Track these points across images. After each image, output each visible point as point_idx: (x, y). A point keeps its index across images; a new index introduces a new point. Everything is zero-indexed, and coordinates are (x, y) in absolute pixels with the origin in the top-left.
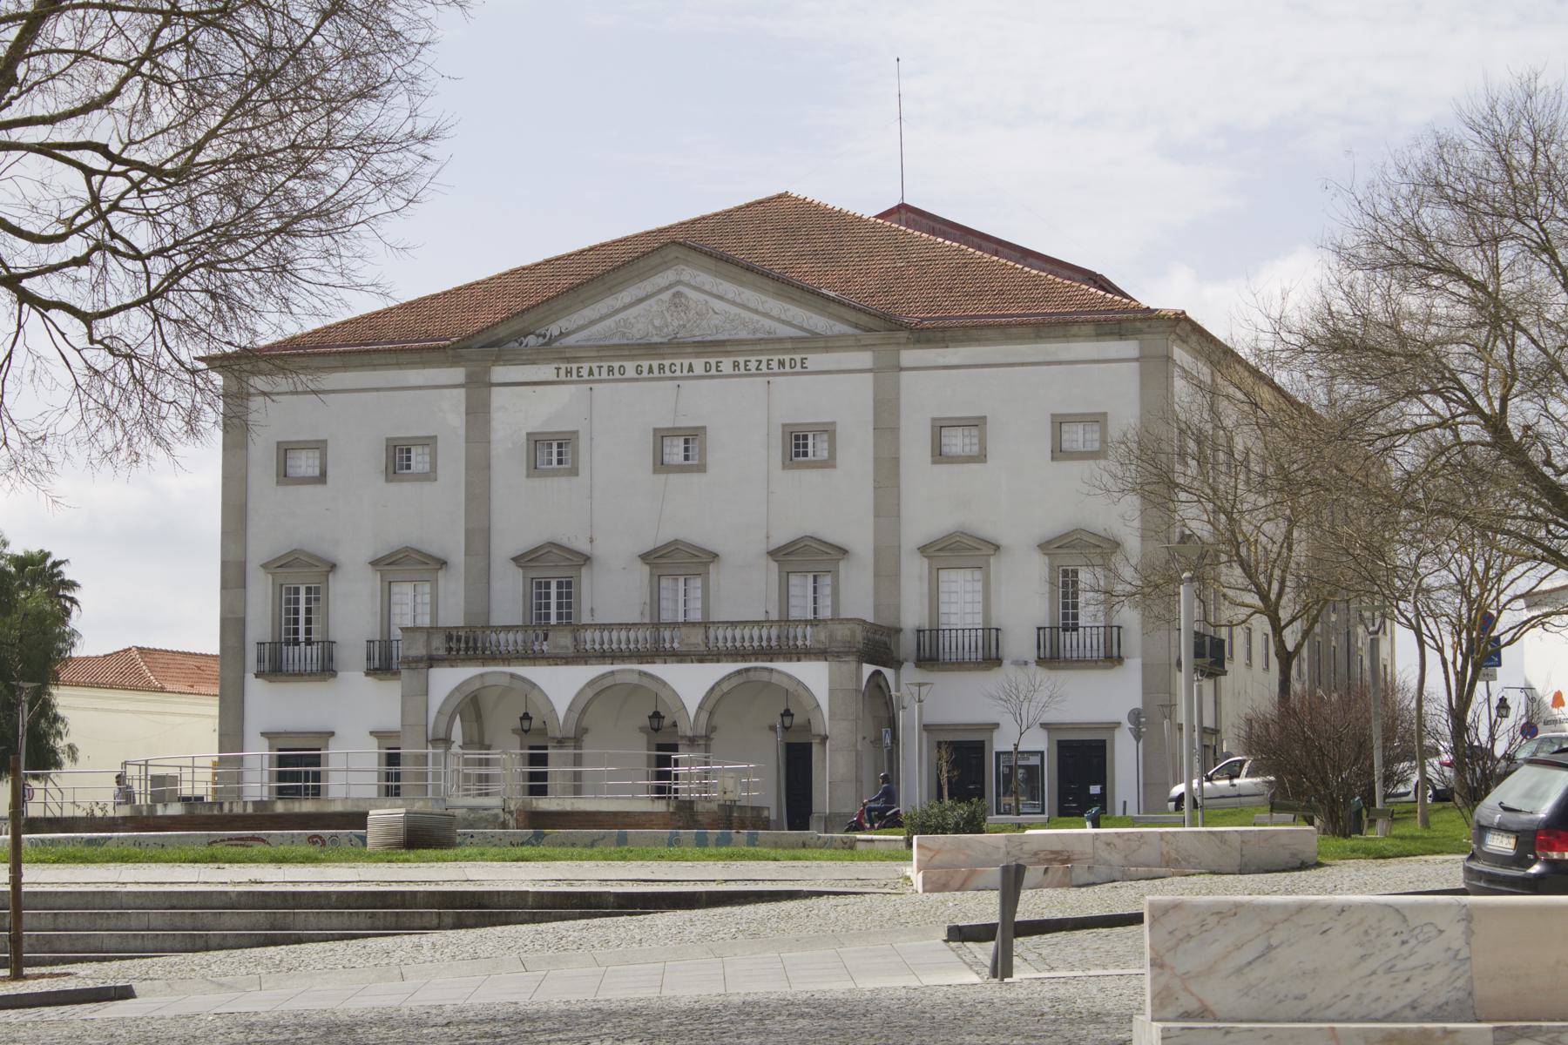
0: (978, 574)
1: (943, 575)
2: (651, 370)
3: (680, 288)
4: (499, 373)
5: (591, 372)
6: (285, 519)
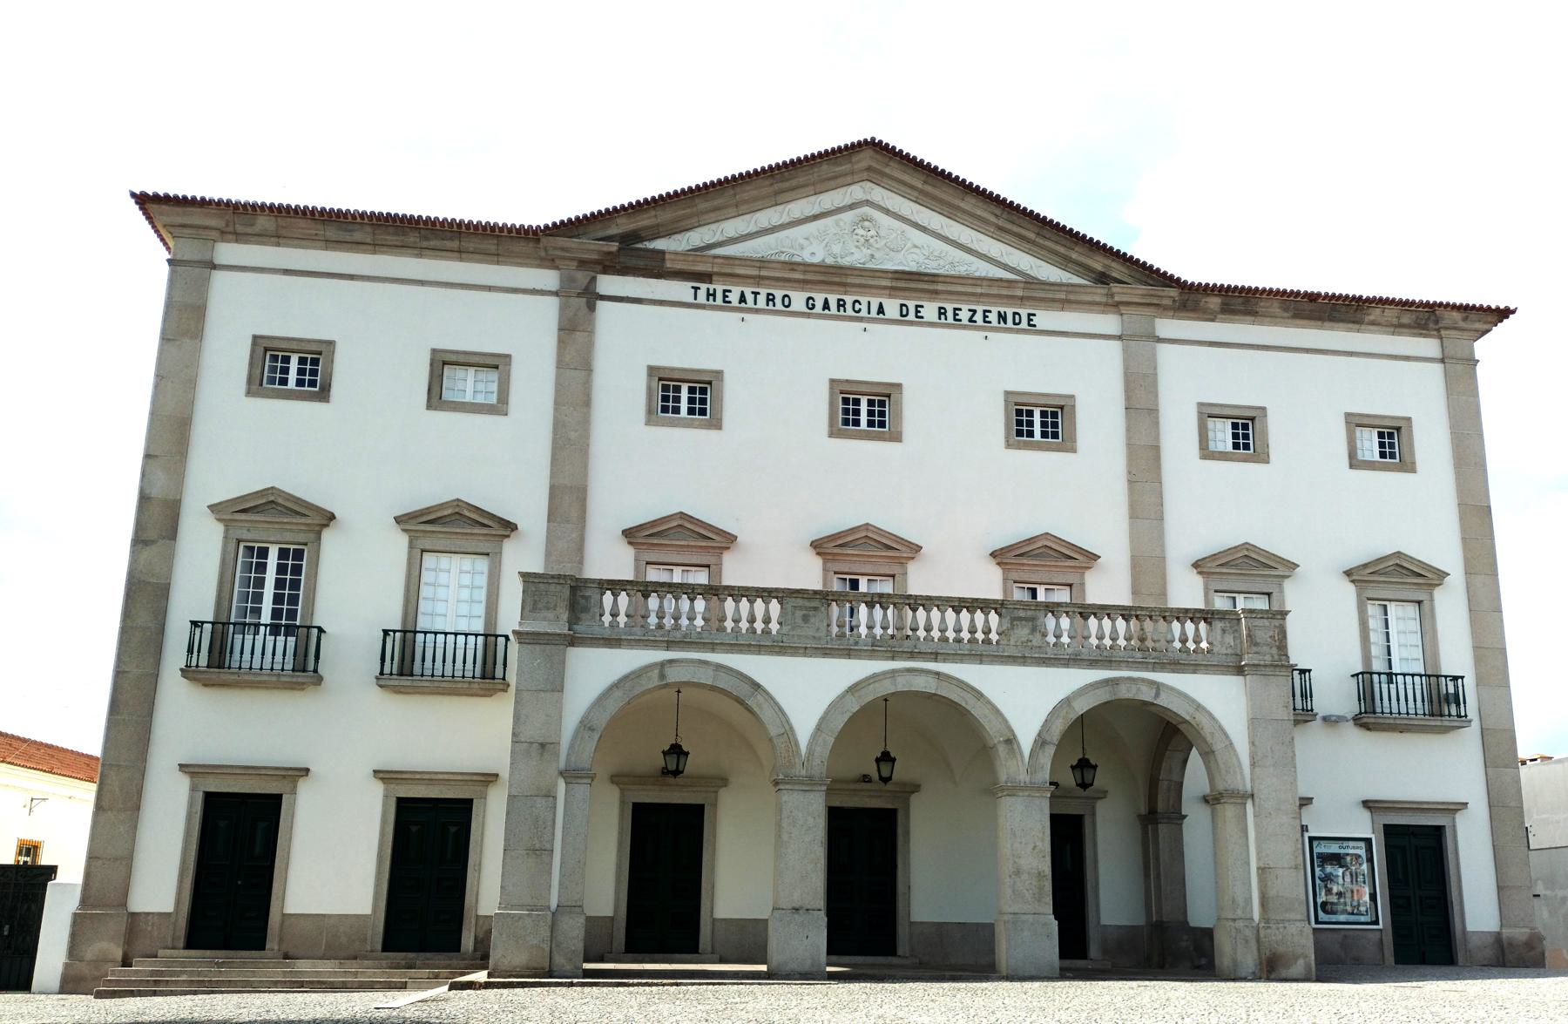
0: (482, 564)
1: (429, 560)
2: (826, 306)
3: (866, 210)
5: (743, 299)
6: (249, 441)
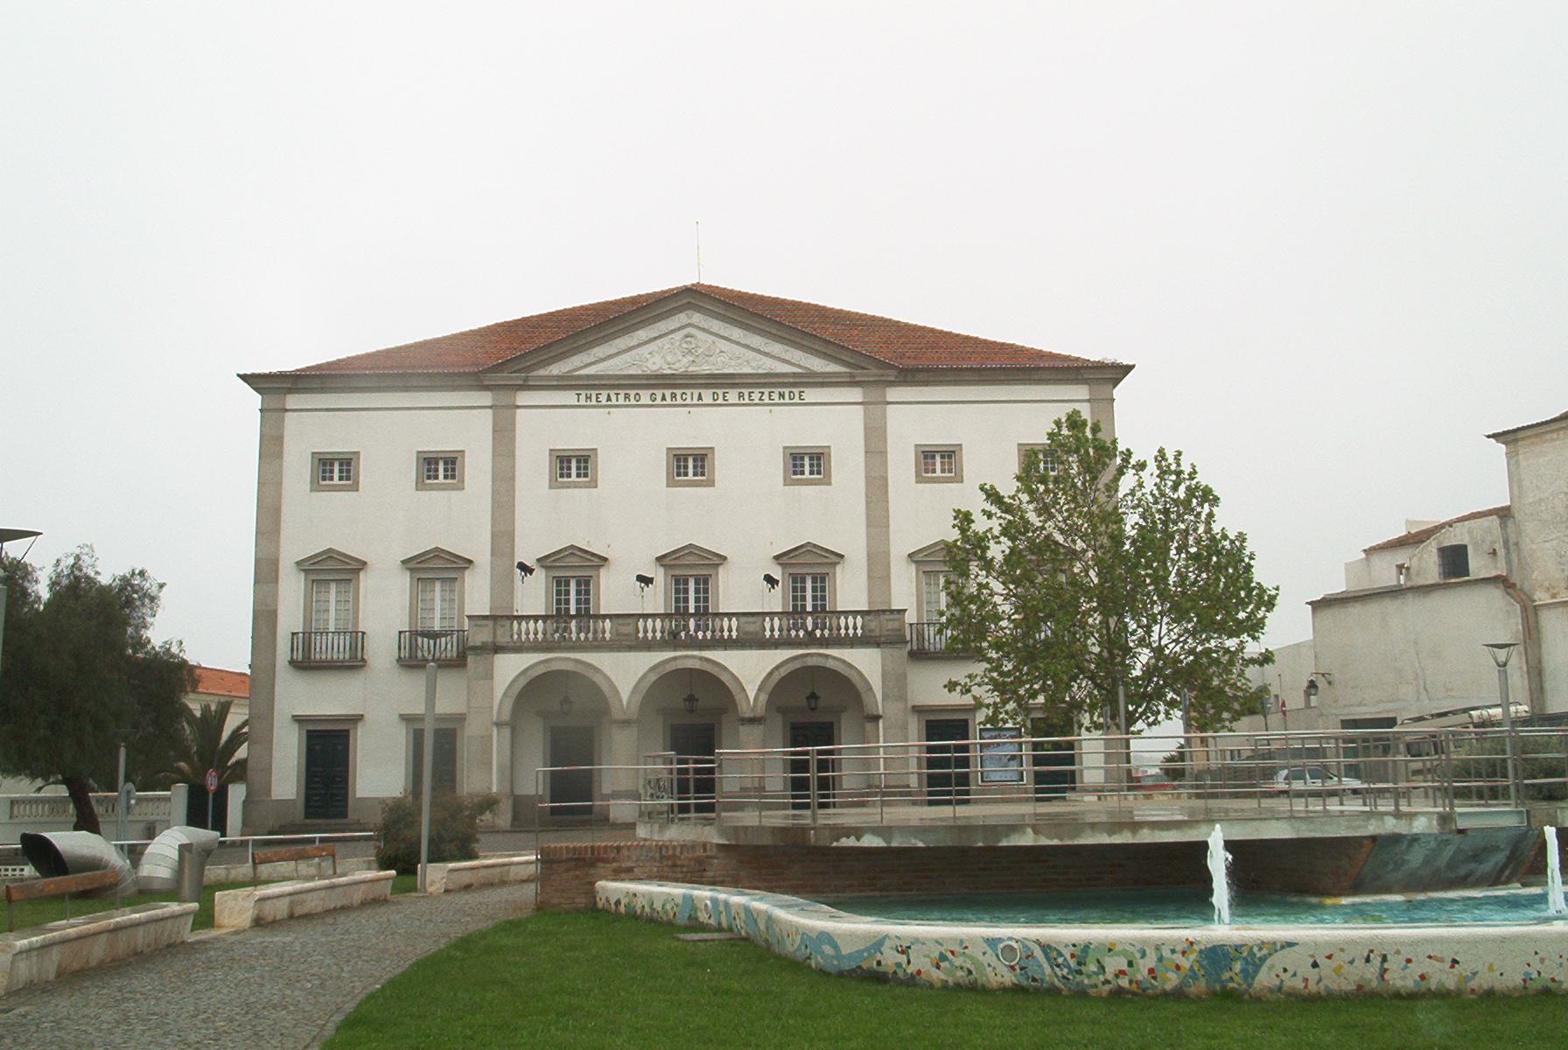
2: (664, 398)
4: (523, 398)
5: (609, 399)
6: (319, 521)
